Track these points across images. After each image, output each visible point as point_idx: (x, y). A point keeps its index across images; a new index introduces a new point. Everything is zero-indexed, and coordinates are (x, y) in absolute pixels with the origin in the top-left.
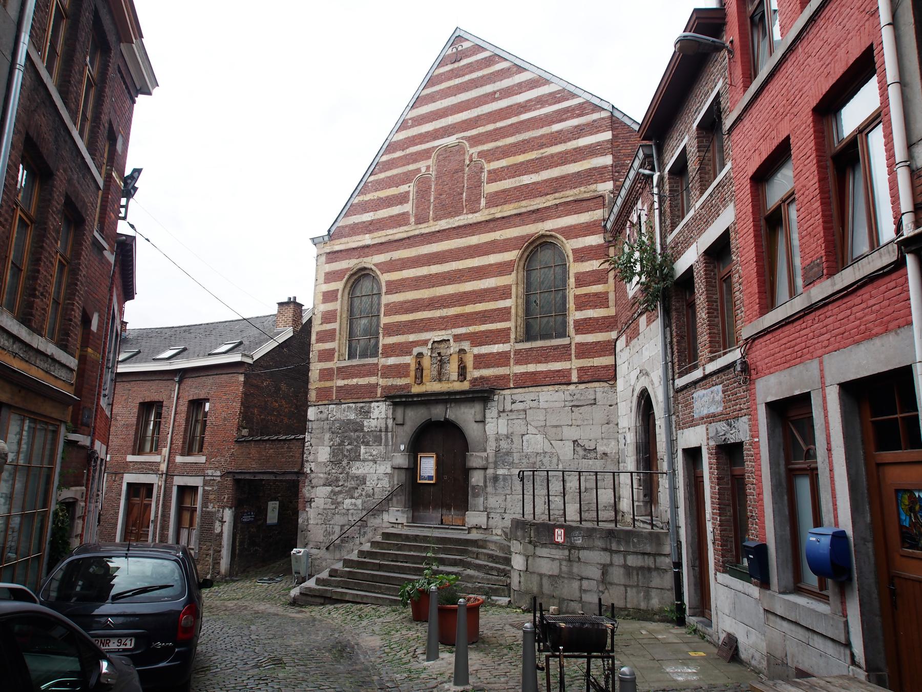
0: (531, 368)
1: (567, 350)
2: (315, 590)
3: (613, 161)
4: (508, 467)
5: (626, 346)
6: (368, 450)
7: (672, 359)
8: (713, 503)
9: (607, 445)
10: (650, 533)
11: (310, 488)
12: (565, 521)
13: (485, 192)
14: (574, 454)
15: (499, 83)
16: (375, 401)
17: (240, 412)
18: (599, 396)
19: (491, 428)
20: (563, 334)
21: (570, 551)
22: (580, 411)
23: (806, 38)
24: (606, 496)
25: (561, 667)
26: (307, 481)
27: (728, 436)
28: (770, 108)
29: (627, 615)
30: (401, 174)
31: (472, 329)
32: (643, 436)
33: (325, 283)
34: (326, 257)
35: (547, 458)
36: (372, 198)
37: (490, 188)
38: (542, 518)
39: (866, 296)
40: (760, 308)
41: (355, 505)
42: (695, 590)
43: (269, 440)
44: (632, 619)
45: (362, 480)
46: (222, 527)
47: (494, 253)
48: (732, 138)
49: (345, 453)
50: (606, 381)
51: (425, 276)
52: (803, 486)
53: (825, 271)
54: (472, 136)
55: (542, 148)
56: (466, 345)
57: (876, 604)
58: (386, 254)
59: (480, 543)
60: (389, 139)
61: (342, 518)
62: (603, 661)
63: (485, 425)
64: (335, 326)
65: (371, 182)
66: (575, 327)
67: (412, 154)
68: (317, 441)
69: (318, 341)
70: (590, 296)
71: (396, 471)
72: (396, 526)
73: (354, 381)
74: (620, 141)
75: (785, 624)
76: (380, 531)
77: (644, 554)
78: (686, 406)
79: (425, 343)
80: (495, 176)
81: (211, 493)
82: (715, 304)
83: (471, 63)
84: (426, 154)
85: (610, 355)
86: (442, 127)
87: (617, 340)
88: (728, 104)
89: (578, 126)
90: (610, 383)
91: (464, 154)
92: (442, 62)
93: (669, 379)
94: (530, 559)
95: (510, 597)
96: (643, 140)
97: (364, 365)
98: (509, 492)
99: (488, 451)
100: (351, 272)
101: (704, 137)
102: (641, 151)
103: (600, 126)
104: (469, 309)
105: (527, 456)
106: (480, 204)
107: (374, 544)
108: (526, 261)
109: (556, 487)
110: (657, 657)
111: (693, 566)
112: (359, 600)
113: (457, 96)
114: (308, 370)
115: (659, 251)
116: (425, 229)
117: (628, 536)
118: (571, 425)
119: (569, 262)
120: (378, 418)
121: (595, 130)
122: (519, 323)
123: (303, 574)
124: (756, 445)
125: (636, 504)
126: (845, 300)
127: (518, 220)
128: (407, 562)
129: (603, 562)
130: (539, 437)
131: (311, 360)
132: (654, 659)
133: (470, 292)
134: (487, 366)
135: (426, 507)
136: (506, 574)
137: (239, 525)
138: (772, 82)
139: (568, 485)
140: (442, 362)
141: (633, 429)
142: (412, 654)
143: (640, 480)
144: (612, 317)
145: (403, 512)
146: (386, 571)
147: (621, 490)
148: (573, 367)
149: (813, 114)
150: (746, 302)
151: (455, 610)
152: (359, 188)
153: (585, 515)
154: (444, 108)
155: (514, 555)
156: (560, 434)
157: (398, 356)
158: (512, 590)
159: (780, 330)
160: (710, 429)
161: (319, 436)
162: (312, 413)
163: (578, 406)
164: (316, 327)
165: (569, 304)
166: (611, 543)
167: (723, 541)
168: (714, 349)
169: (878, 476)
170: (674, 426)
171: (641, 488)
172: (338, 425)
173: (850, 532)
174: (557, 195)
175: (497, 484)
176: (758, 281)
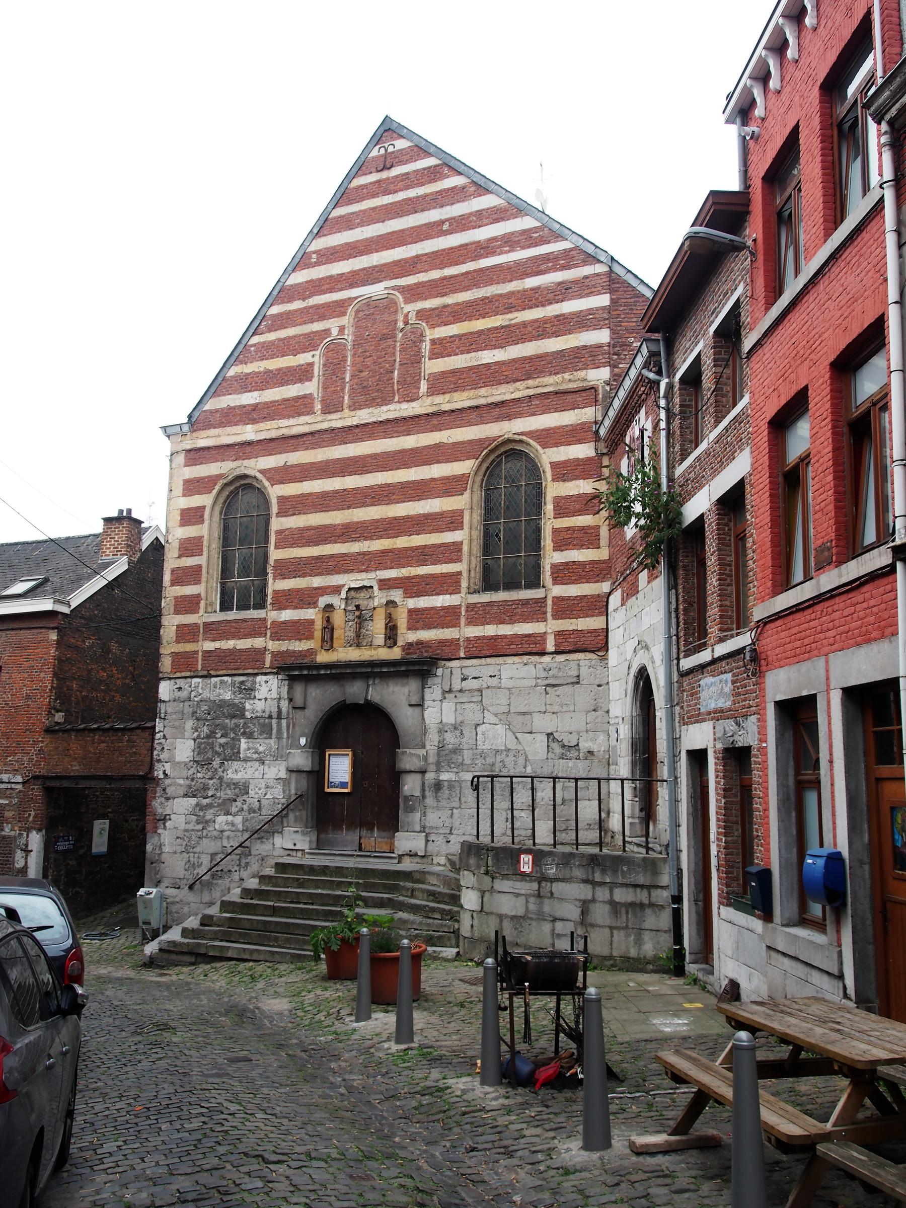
0: (490, 630)
1: (541, 607)
2: (181, 944)
3: (612, 338)
4: (455, 770)
5: (622, 605)
6: (251, 745)
7: (678, 632)
8: (718, 820)
9: (594, 740)
10: (644, 859)
11: (163, 800)
12: (534, 844)
13: (427, 372)
14: (548, 752)
15: (448, 208)
16: (262, 674)
17: (52, 687)
18: (584, 672)
19: (431, 715)
20: (535, 582)
21: (539, 883)
22: (558, 693)
23: (828, 275)
24: (588, 810)
25: (527, 1005)
26: (158, 789)
27: (736, 738)
28: (790, 343)
29: (612, 966)
30: (300, 335)
31: (405, 572)
32: (641, 730)
33: (184, 495)
34: (186, 456)
35: (511, 758)
36: (257, 370)
37: (433, 366)
38: (503, 839)
39: (868, 595)
40: (774, 586)
41: (233, 824)
42: (698, 930)
43: (98, 729)
44: (619, 970)
45: (243, 788)
46: (26, 858)
47: (438, 462)
48: (751, 365)
49: (217, 749)
50: (593, 652)
51: (337, 492)
52: (811, 798)
53: (834, 558)
54: (408, 286)
55: (511, 312)
56: (396, 595)
57: (870, 931)
58: (278, 456)
59: (417, 876)
60: (283, 280)
61: (213, 844)
62: (574, 999)
63: (423, 710)
64: (201, 560)
65: (254, 345)
66: (552, 573)
67: (317, 307)
68: (174, 730)
69: (174, 583)
70: (574, 531)
71: (294, 775)
72: (294, 853)
73: (230, 644)
74: (622, 308)
75: (786, 961)
76: (273, 862)
77: (636, 886)
78: (692, 695)
79: (336, 590)
80: (442, 348)
81: (7, 808)
82: (728, 568)
83: (408, 174)
84: (338, 309)
85: (600, 614)
86: (364, 269)
87: (610, 594)
88: (749, 319)
89: (562, 283)
90: (600, 654)
91: (396, 312)
92: (364, 168)
93: (672, 659)
94: (487, 895)
95: (458, 946)
96: (647, 332)
97: (245, 620)
98: (456, 804)
99: (428, 747)
100: (225, 482)
101: (722, 347)
102: (644, 346)
103: (594, 286)
104: (402, 542)
105: (482, 755)
106: (419, 388)
107: (263, 879)
108: (484, 476)
109: (522, 797)
110: (643, 1009)
111: (696, 901)
112: (247, 957)
113: (386, 222)
114: (158, 626)
115: (664, 488)
116: (336, 421)
117: (615, 863)
118: (545, 712)
119: (546, 481)
120: (266, 699)
121: (586, 292)
122: (473, 566)
123: (155, 924)
124: (763, 751)
125: (627, 821)
126: (851, 595)
127: (473, 416)
128: (312, 904)
129: (582, 897)
130: (501, 729)
131: (164, 611)
132: (640, 1012)
133: (403, 518)
134: (428, 626)
135: (337, 826)
136: (454, 917)
137: (52, 855)
138: (794, 312)
139: (539, 795)
140: (361, 618)
141: (628, 719)
142: (334, 1016)
143: (635, 788)
144: (604, 561)
145: (304, 834)
146: (283, 917)
147: (611, 801)
148: (549, 631)
149: (830, 369)
150: (760, 576)
151: (397, 959)
152: (236, 354)
153: (561, 837)
154: (367, 239)
155: (464, 890)
156: (529, 724)
157: (296, 608)
158: (461, 938)
159: (791, 618)
160: (718, 728)
161: (177, 724)
162: (165, 690)
163: (554, 686)
164: (171, 561)
165: (545, 541)
166: (593, 873)
167: (728, 867)
168: (726, 627)
169: (877, 792)
170: (677, 720)
171: (637, 799)
172: (206, 707)
173: (846, 854)
174: (530, 382)
175: (440, 794)
176: (772, 552)
